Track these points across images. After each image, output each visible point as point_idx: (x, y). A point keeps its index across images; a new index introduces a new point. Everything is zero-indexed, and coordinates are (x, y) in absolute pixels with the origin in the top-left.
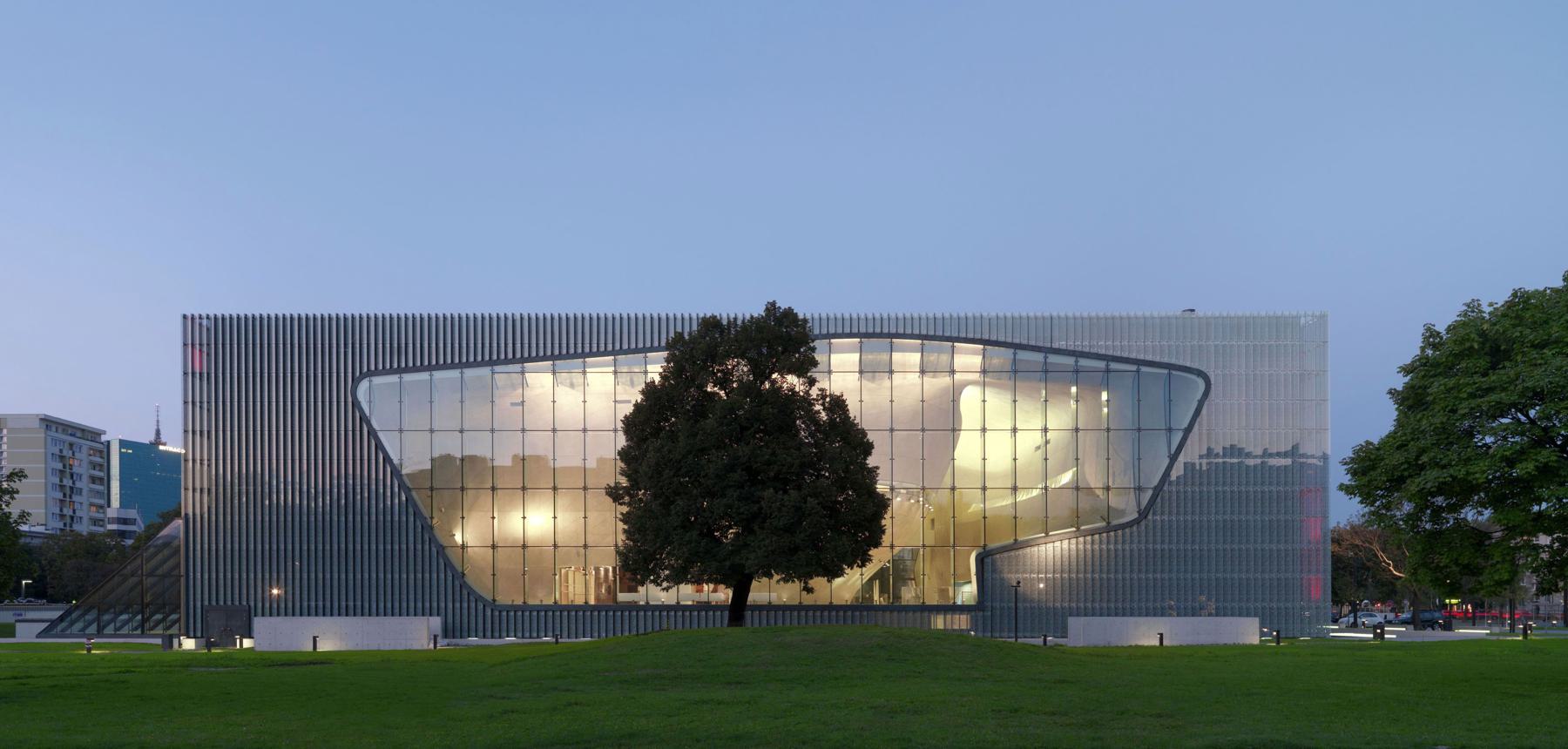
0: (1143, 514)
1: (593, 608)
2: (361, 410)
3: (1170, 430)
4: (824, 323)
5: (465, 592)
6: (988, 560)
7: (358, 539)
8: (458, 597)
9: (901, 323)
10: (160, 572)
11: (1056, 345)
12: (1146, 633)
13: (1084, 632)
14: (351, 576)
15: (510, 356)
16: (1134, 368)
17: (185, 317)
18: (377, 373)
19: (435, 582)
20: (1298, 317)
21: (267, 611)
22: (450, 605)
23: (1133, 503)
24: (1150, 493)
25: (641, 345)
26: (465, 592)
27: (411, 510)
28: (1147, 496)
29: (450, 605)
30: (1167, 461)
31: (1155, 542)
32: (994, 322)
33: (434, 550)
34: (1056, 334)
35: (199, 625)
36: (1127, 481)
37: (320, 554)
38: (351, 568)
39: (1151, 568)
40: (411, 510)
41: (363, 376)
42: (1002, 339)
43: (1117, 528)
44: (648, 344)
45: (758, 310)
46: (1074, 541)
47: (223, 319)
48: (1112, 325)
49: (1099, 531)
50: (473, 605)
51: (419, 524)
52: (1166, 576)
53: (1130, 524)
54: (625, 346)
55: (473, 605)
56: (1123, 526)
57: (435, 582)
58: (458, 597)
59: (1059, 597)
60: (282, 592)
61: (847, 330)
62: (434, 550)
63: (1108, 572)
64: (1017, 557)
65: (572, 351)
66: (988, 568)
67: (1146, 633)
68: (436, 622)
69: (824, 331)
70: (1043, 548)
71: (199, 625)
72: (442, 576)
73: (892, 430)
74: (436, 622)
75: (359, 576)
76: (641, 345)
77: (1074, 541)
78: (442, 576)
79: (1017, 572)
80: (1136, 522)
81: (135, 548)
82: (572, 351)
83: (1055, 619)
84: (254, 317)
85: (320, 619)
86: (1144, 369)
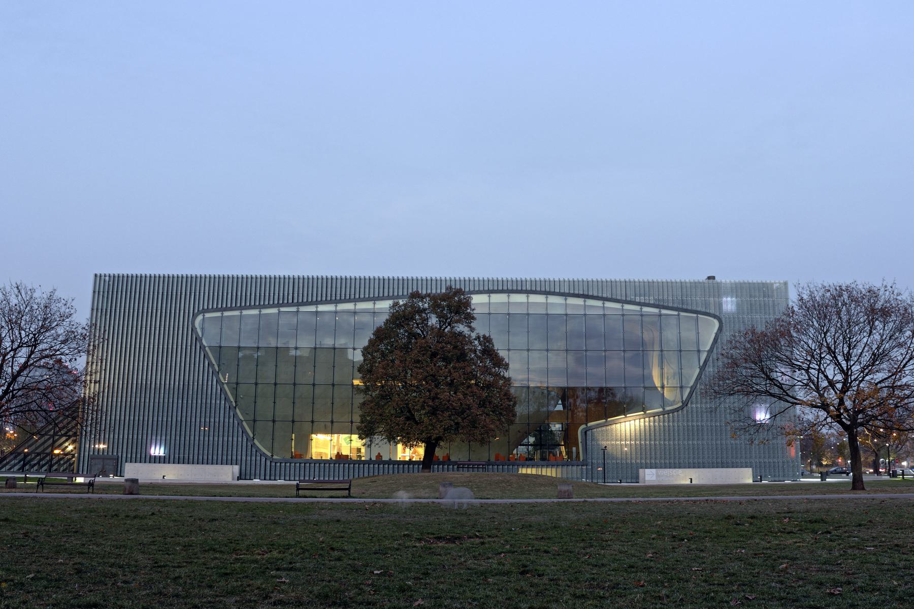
0: (685, 404)
1: (364, 462)
2: (197, 333)
3: (699, 351)
4: (486, 283)
5: (254, 450)
7: (165, 414)
8: (249, 453)
11: (628, 299)
13: (650, 476)
14: (183, 439)
15: (290, 301)
16: (676, 313)
17: (96, 275)
20: (772, 284)
22: (244, 458)
23: (679, 396)
24: (688, 390)
26: (254, 450)
27: (223, 396)
28: (687, 392)
29: (244, 458)
30: (698, 370)
31: (692, 421)
33: (236, 422)
34: (628, 292)
36: (675, 383)
37: (165, 423)
38: (140, 432)
40: (223, 396)
41: (199, 312)
42: (595, 294)
43: (668, 412)
44: (376, 295)
45: (702, 278)
46: (642, 420)
47: (137, 276)
48: (651, 284)
49: (658, 414)
50: (258, 458)
51: (227, 405)
52: (700, 442)
53: (677, 410)
54: (362, 296)
55: (258, 458)
56: (673, 411)
57: (235, 443)
58: (249, 453)
59: (634, 456)
60: (105, 446)
61: (500, 288)
62: (236, 422)
63: (650, 440)
64: (612, 430)
67: (683, 477)
68: (236, 468)
69: (477, 289)
70: (618, 425)
72: (240, 439)
73: (528, 350)
74: (236, 468)
75: (135, 437)
76: (372, 295)
77: (642, 420)
78: (240, 439)
79: (607, 440)
80: (682, 408)
81: (527, 434)
82: (329, 298)
84: (137, 276)
85: (166, 465)
86: (682, 314)
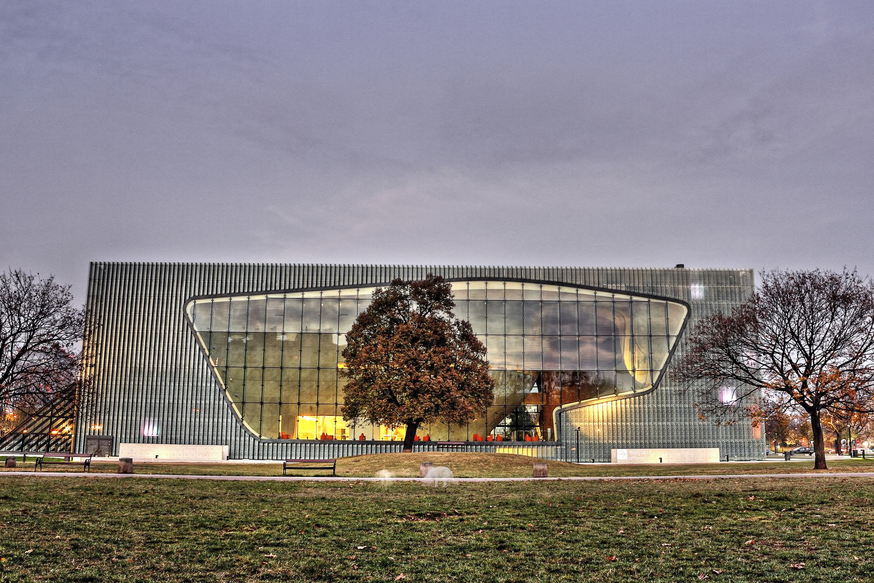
0: (655, 387)
2: (188, 319)
6: (563, 414)
9: (479, 272)
10: (45, 418)
12: (652, 457)
13: (622, 456)
15: (278, 288)
16: (646, 300)
17: (92, 263)
18: (199, 297)
19: (225, 424)
20: (738, 272)
21: (128, 440)
23: (649, 381)
25: (346, 284)
26: (243, 431)
28: (657, 375)
30: (667, 355)
31: (662, 403)
32: (609, 272)
33: (226, 404)
35: (82, 447)
39: (665, 419)
40: (213, 379)
41: (191, 299)
42: (569, 281)
43: (639, 395)
49: (629, 397)
50: (247, 439)
53: (647, 392)
54: (346, 284)
55: (247, 439)
57: (225, 424)
65: (314, 286)
66: (563, 419)
67: (652, 457)
68: (226, 448)
71: (82, 447)
72: (229, 420)
73: (505, 335)
74: (226, 448)
76: (355, 283)
78: (229, 420)
80: (652, 391)
83: (604, 450)
86: (652, 300)
